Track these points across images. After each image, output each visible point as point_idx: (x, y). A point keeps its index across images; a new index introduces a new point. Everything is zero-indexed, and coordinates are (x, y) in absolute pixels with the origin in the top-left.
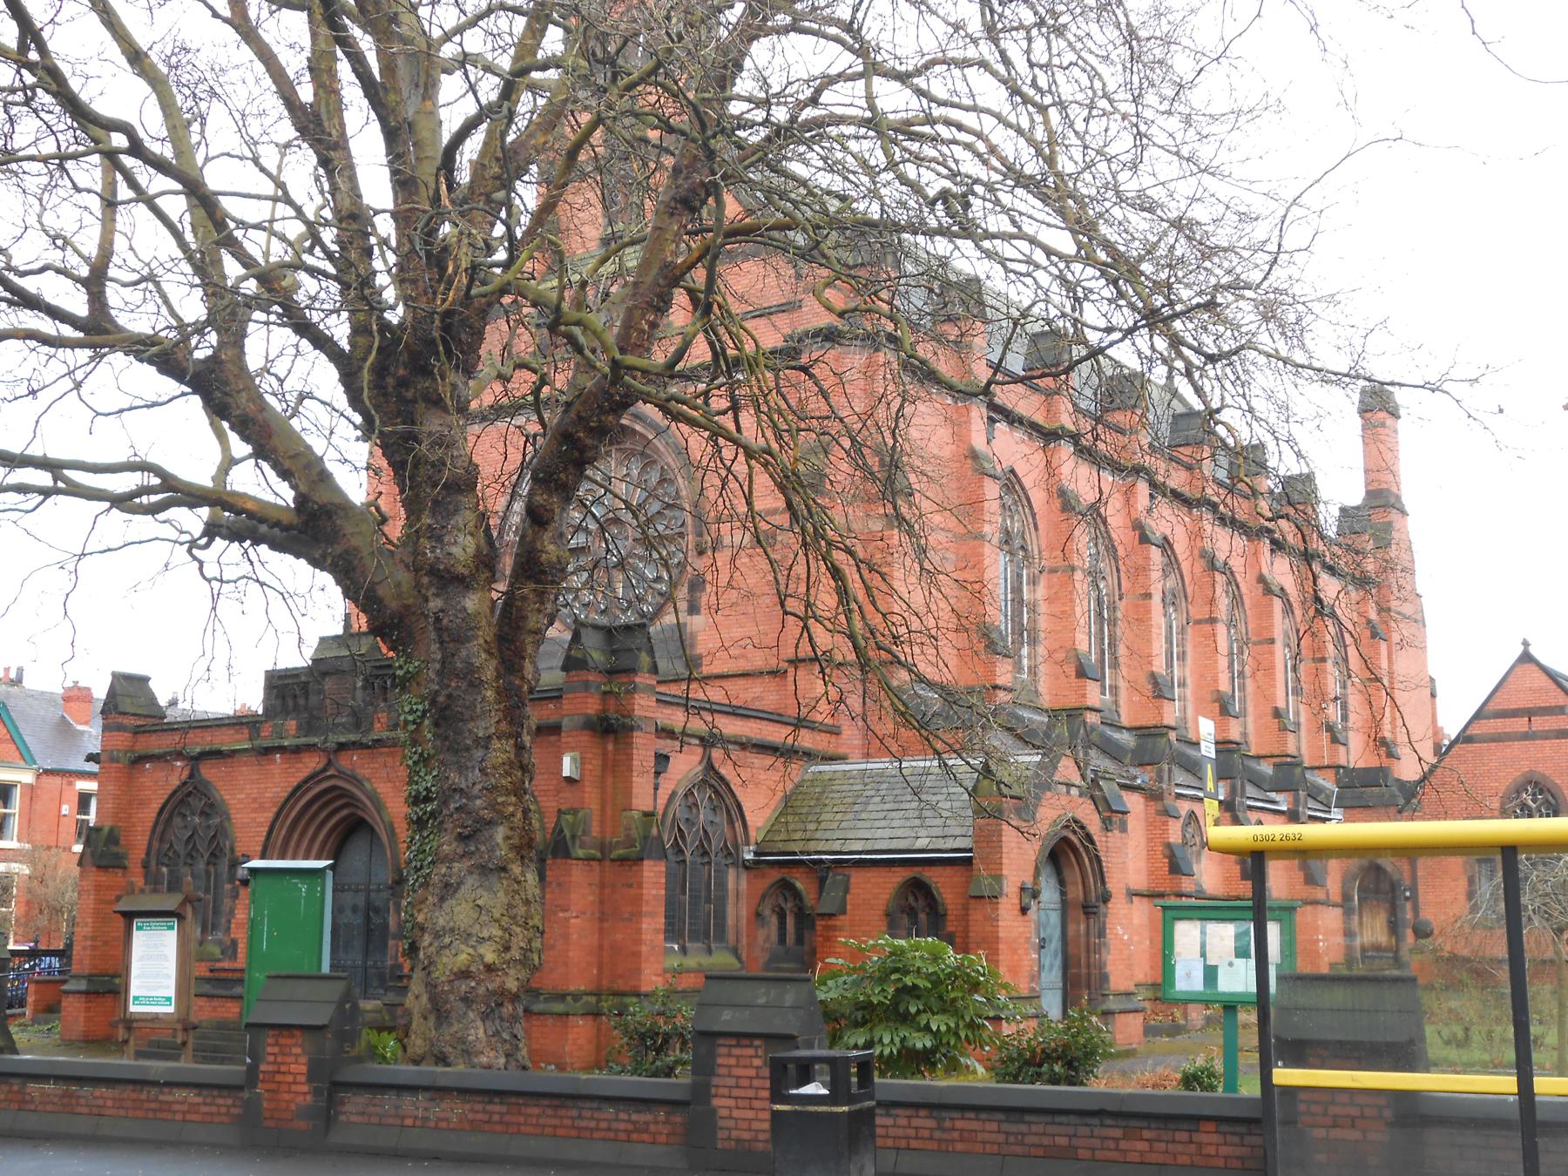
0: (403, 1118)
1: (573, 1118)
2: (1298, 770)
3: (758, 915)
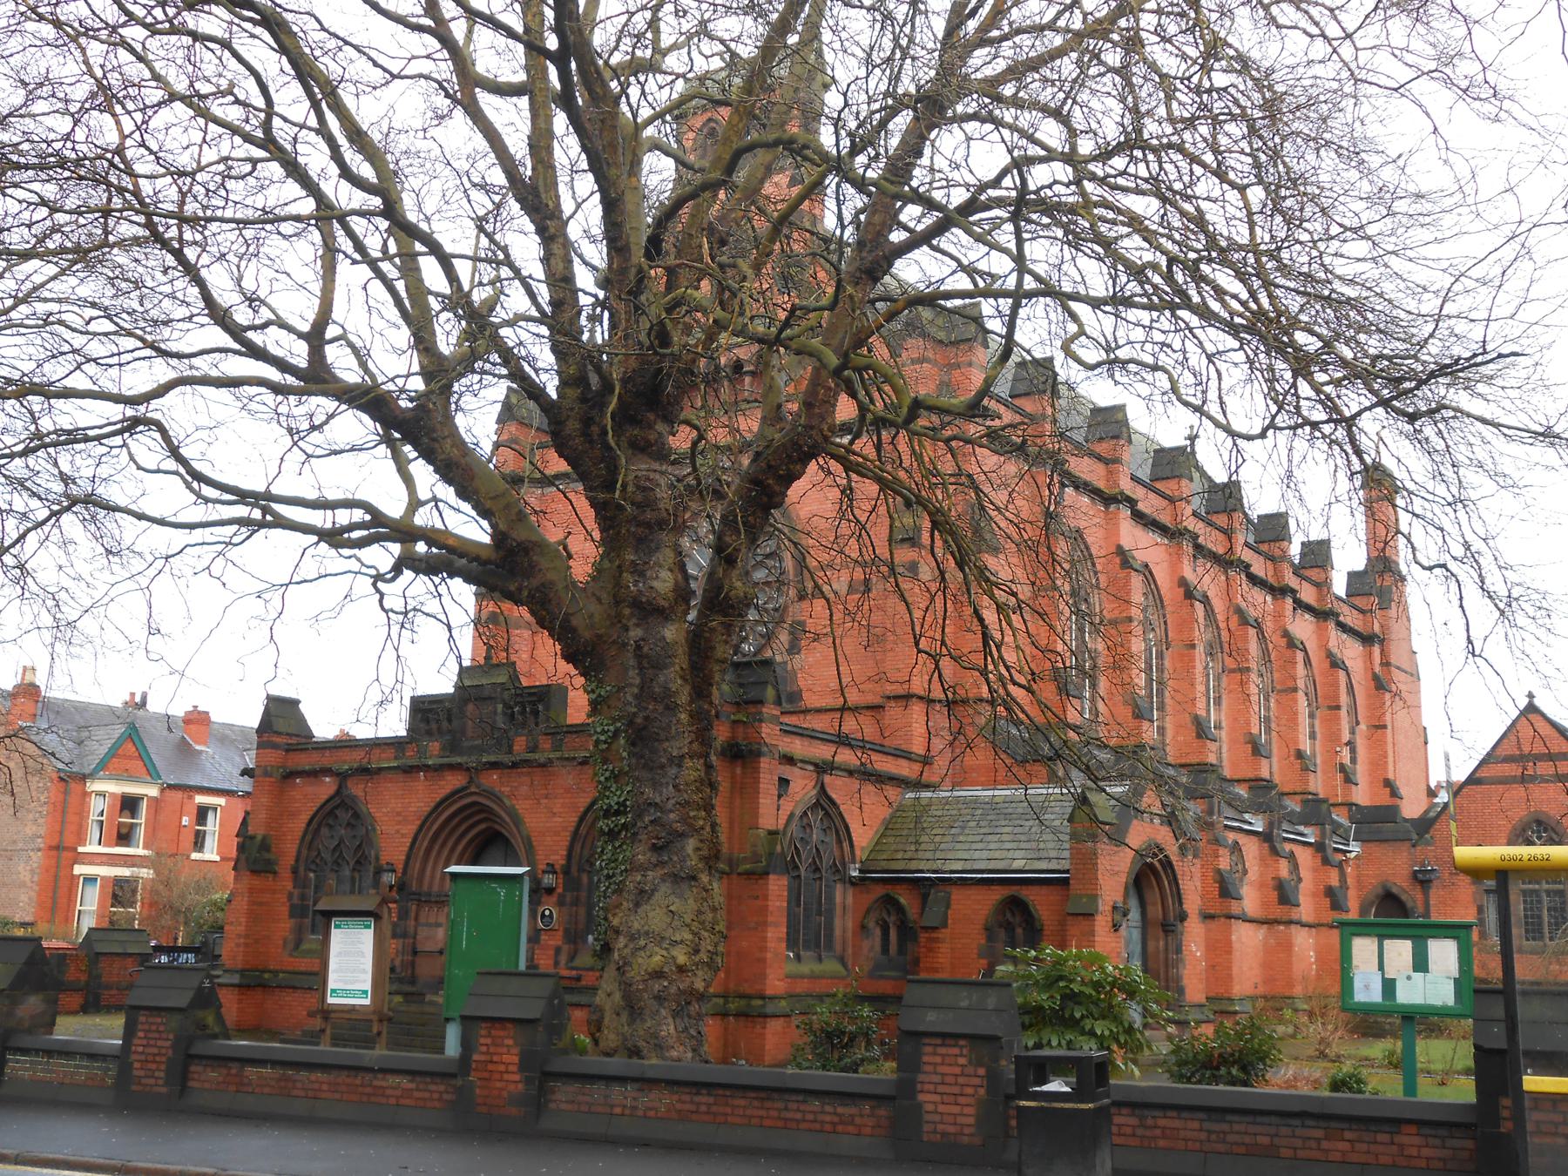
0: (612, 1106)
1: (779, 1110)
2: (1324, 807)
3: (863, 927)
